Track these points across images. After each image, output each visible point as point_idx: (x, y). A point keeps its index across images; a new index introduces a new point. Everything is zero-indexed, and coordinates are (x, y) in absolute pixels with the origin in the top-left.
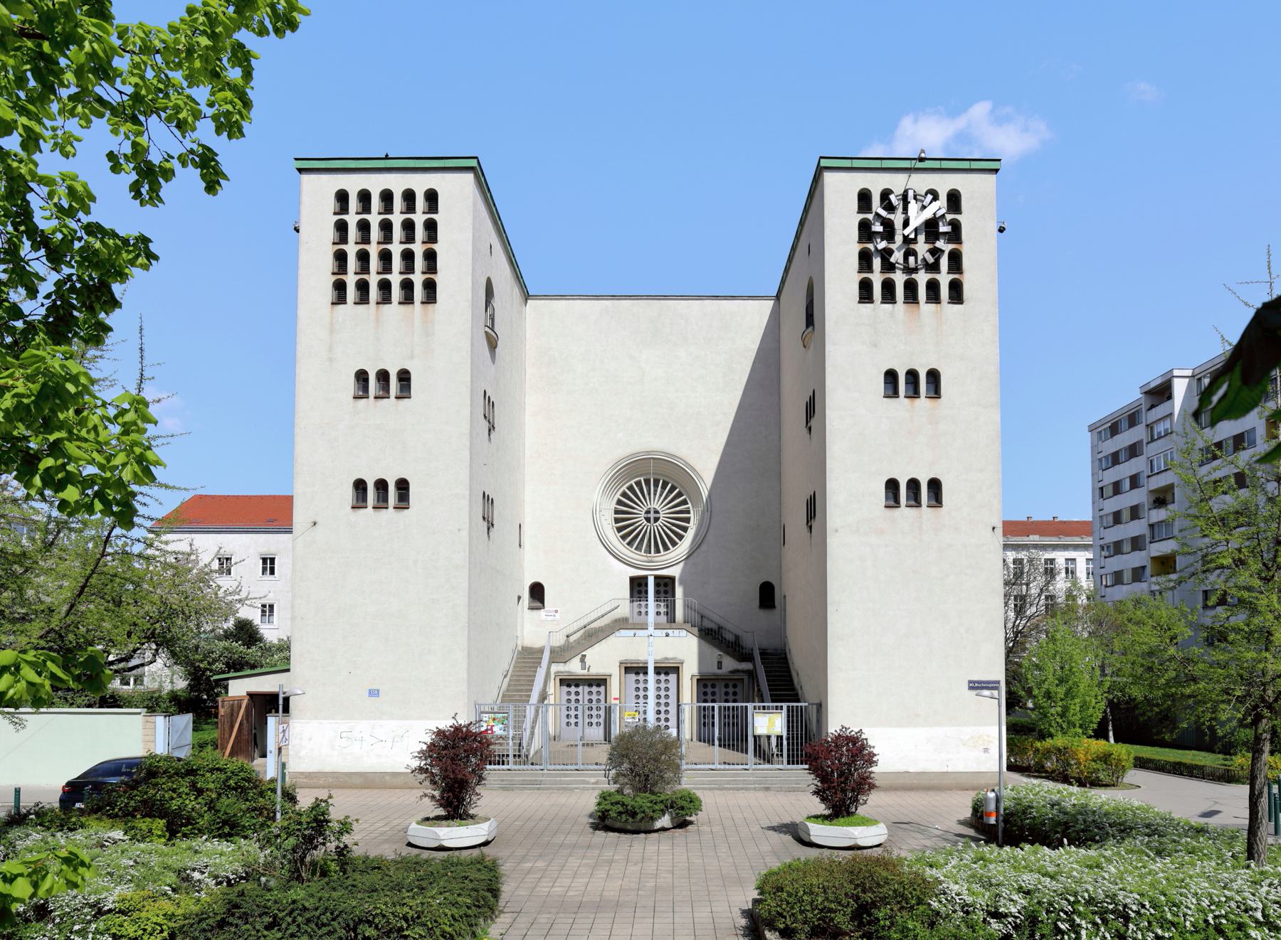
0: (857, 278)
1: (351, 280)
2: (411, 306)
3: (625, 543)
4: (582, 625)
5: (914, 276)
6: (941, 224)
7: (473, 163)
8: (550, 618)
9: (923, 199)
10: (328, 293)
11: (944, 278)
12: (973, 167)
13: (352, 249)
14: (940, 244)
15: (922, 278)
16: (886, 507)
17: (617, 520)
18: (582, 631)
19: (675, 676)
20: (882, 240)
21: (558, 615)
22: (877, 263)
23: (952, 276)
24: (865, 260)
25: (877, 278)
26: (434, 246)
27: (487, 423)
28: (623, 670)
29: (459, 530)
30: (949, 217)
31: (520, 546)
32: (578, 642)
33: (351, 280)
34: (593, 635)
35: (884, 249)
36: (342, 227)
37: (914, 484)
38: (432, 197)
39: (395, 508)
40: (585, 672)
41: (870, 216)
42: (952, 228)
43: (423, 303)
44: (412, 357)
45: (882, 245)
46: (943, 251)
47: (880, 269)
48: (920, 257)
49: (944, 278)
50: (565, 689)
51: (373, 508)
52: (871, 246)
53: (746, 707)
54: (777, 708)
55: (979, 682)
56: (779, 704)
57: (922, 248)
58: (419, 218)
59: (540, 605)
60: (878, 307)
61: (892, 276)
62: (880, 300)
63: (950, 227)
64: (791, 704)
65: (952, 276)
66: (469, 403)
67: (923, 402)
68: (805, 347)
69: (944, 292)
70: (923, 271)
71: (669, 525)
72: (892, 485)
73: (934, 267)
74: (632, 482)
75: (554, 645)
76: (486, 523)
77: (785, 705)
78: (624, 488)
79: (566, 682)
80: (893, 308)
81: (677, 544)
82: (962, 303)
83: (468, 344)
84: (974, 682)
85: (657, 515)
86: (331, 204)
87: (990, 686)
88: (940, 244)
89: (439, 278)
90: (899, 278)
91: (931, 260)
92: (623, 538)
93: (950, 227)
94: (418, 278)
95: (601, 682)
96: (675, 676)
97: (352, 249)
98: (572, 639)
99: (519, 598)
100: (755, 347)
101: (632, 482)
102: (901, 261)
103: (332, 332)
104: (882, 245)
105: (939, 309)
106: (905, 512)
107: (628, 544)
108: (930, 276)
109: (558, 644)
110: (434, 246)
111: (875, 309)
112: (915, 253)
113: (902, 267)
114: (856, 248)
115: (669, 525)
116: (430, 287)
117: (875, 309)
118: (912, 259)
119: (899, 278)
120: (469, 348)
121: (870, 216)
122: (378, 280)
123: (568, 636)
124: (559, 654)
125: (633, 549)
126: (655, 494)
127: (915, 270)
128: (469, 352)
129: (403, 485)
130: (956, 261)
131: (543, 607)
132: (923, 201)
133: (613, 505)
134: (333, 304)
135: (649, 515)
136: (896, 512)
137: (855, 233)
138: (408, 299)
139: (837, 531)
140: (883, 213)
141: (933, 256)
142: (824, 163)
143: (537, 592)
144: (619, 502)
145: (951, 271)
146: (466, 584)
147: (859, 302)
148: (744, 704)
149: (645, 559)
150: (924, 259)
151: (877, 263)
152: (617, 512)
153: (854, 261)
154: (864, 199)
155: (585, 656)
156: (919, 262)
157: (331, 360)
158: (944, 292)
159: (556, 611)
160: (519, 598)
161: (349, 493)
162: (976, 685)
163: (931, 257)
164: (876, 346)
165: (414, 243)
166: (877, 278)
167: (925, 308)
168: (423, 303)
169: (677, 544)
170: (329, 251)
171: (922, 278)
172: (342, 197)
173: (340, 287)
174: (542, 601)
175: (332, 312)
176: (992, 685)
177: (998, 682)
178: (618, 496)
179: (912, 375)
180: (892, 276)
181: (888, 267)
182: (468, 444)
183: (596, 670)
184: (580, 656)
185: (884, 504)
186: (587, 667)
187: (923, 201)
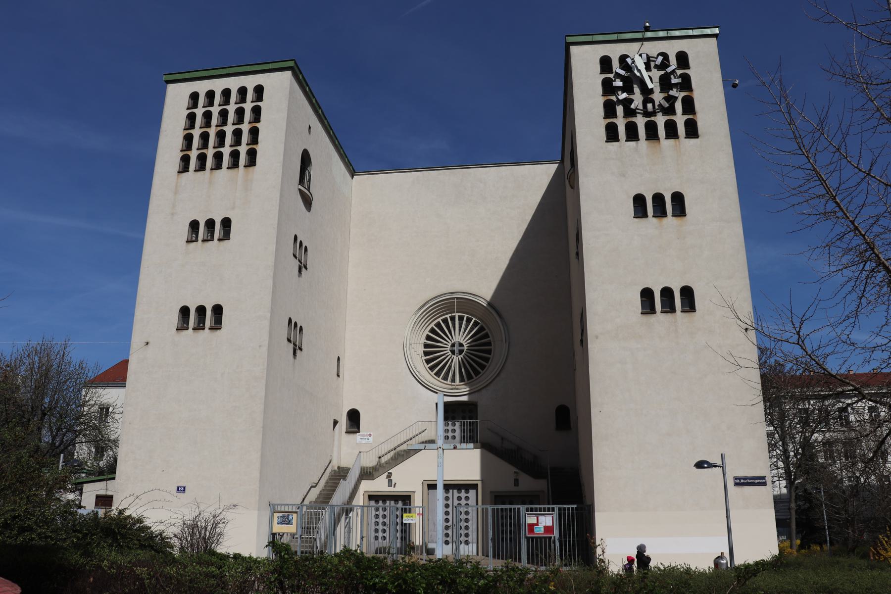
0: (603, 123)
1: (194, 154)
2: (236, 169)
3: (427, 366)
4: (393, 447)
5: (653, 118)
6: (672, 77)
7: (292, 64)
8: (364, 441)
9: (655, 59)
10: (176, 163)
11: (680, 119)
12: (695, 34)
13: (196, 133)
14: (673, 92)
15: (660, 120)
16: (642, 313)
17: (426, 354)
18: (392, 453)
19: (475, 491)
20: (623, 93)
21: (371, 438)
22: (620, 110)
23: (686, 117)
24: (609, 110)
25: (621, 123)
26: (258, 125)
27: (298, 263)
28: (426, 487)
29: (260, 346)
30: (679, 72)
31: (338, 376)
32: (387, 463)
33: (194, 154)
34: (401, 456)
35: (625, 99)
36: (191, 117)
37: (667, 293)
38: (259, 91)
39: (209, 329)
40: (392, 489)
41: (611, 76)
42: (682, 80)
43: (245, 166)
44: (233, 208)
45: (623, 96)
46: (676, 98)
47: (623, 115)
48: (657, 103)
49: (680, 119)
50: (373, 503)
51: (193, 329)
52: (614, 98)
53: (519, 509)
54: (549, 510)
55: (745, 478)
56: (551, 506)
57: (658, 97)
58: (248, 106)
59: (356, 430)
60: (624, 146)
61: (634, 119)
62: (625, 139)
63: (680, 79)
64: (562, 506)
65: (686, 117)
66: (275, 241)
67: (670, 220)
68: (572, 188)
69: (681, 130)
70: (661, 114)
71: (469, 355)
72: (647, 294)
73: (671, 111)
74: (440, 320)
75: (365, 465)
76: (292, 345)
77: (556, 507)
78: (432, 325)
79: (372, 497)
80: (637, 144)
81: (479, 373)
82: (698, 137)
83: (278, 195)
84: (740, 478)
85: (461, 348)
86: (185, 101)
87: (756, 481)
88: (673, 92)
89: (259, 148)
90: (640, 121)
91: (666, 105)
92: (432, 368)
93: (680, 79)
94: (243, 149)
95: (406, 499)
96: (475, 491)
97: (196, 133)
98: (384, 460)
99: (335, 423)
100: (539, 201)
101: (440, 320)
102: (641, 107)
103: (176, 192)
104: (623, 96)
105: (678, 143)
106: (660, 318)
107: (436, 374)
108: (667, 118)
109: (371, 465)
110: (258, 125)
111: (620, 147)
112: (652, 101)
113: (642, 112)
114: (601, 100)
115: (469, 355)
116: (252, 155)
117: (620, 147)
118: (650, 106)
119: (640, 121)
120: (278, 199)
121: (611, 76)
122: (214, 152)
123: (380, 458)
124: (367, 474)
125: (433, 374)
126: (460, 330)
127: (654, 113)
128: (278, 201)
129: (218, 310)
130: (689, 106)
131: (359, 432)
132: (655, 61)
133: (423, 340)
134: (179, 172)
135: (453, 348)
136: (652, 318)
137: (599, 89)
138: (235, 165)
139: (597, 337)
140: (622, 72)
141: (668, 103)
142: (569, 39)
143: (354, 417)
144: (428, 338)
145: (685, 112)
146: (263, 394)
147: (606, 142)
148: (516, 507)
149: (450, 387)
150: (660, 105)
151: (620, 110)
152: (426, 346)
153: (601, 111)
154: (605, 63)
155: (391, 473)
156: (657, 107)
157: (173, 214)
158: (681, 130)
159: (370, 435)
160: (335, 423)
161: (174, 317)
162: (742, 481)
163: (666, 103)
164: (624, 176)
165: (243, 124)
166: (621, 123)
167: (666, 144)
168: (245, 166)
169: (480, 373)
170: (180, 134)
171: (660, 120)
172: (194, 97)
173: (185, 160)
174: (358, 428)
175: (178, 179)
176: (760, 481)
177: (764, 478)
178: (427, 332)
179: (658, 199)
180: (634, 119)
181: (630, 112)
182: (272, 274)
183: (401, 488)
184: (386, 474)
185: (640, 311)
186: (393, 484)
187: (655, 61)
